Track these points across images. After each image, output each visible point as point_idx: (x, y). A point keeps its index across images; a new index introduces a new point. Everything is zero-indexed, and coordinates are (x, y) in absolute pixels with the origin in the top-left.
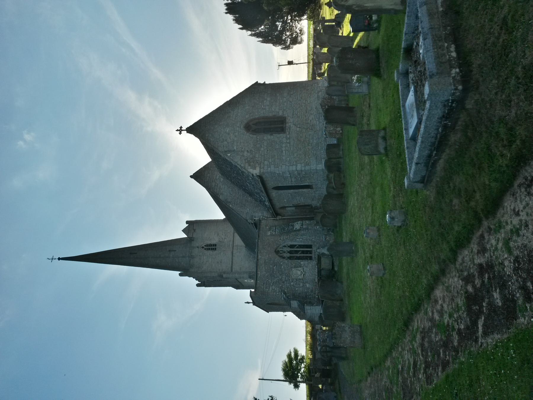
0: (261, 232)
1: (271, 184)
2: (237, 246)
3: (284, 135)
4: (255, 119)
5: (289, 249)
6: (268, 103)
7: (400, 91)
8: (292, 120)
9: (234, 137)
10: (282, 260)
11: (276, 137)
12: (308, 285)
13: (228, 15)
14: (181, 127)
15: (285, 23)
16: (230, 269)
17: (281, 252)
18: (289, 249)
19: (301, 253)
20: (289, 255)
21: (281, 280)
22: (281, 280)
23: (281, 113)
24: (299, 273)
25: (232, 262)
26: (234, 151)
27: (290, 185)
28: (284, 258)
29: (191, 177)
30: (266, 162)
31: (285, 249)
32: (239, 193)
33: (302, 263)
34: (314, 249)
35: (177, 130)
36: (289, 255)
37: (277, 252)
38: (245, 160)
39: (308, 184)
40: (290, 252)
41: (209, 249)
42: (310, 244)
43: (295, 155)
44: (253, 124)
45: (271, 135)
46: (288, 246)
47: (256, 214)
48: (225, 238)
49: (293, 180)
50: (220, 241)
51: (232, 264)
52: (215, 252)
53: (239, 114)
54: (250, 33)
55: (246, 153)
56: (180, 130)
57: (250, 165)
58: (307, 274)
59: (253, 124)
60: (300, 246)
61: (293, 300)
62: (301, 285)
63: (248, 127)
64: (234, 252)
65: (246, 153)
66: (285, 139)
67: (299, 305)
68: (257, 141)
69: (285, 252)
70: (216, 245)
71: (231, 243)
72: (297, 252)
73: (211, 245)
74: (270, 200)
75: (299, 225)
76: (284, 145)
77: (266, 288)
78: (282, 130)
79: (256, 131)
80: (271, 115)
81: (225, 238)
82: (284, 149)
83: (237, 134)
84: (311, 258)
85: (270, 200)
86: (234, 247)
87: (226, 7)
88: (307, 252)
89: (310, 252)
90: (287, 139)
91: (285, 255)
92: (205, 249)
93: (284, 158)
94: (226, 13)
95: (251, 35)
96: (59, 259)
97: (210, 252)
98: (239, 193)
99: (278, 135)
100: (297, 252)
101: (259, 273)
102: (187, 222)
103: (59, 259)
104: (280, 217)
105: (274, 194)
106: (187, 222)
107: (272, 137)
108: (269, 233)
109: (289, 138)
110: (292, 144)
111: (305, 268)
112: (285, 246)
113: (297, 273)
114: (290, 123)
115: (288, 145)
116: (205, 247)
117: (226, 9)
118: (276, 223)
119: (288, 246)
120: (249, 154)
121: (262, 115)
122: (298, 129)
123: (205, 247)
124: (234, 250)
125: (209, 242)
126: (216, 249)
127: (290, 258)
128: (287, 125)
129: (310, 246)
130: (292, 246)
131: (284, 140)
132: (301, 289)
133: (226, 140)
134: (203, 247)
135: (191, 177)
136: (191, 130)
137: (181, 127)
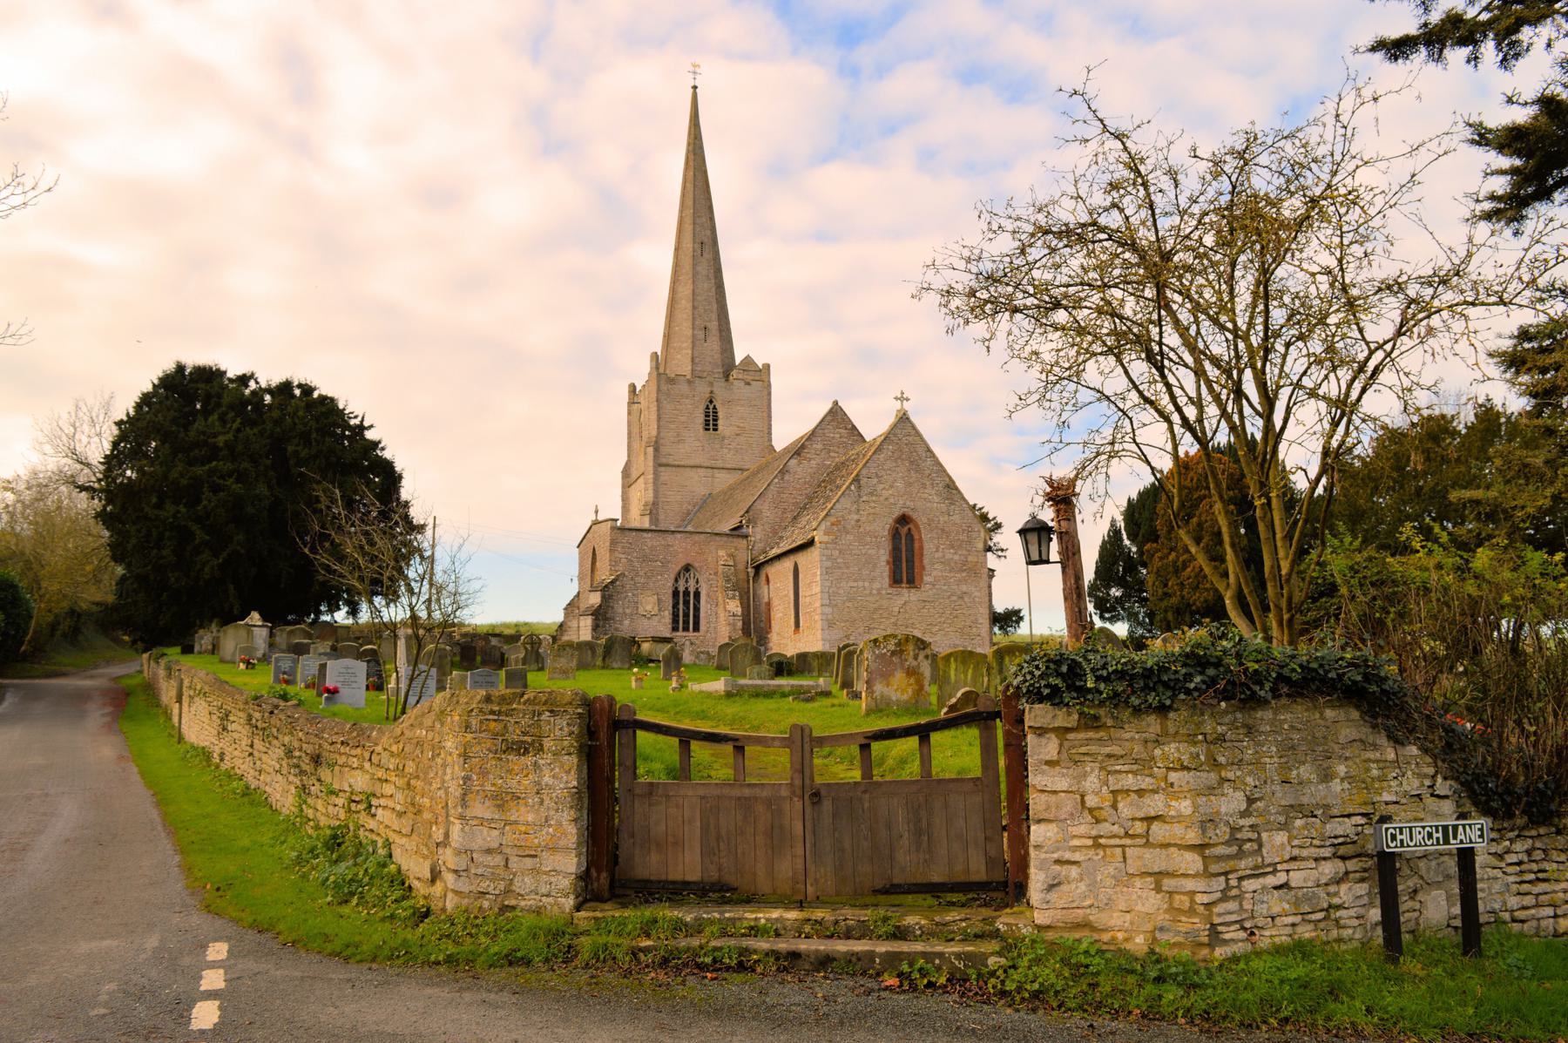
1: (801, 558)
5: (692, 590)
6: (948, 556)
7: (1003, 778)
8: (913, 598)
9: (894, 493)
11: (883, 571)
12: (627, 622)
16: (664, 461)
18: (692, 590)
19: (685, 609)
20: (681, 589)
21: (637, 575)
22: (637, 575)
24: (649, 608)
29: (836, 403)
30: (836, 553)
31: (692, 583)
34: (691, 634)
35: (1468, 61)
36: (681, 589)
37: (687, 568)
40: (686, 593)
42: (703, 627)
47: (758, 529)
56: (902, 398)
60: (697, 609)
61: (603, 597)
63: (904, 520)
71: (719, 464)
72: (686, 603)
73: (715, 420)
74: (779, 557)
78: (896, 580)
79: (895, 535)
80: (926, 561)
84: (675, 629)
85: (779, 557)
88: (686, 622)
89: (686, 629)
91: (681, 583)
93: (843, 584)
96: (695, 87)
97: (701, 419)
99: (886, 574)
100: (686, 603)
102: (767, 367)
103: (695, 87)
105: (787, 564)
106: (767, 367)
113: (648, 604)
114: (906, 595)
118: (741, 567)
121: (926, 546)
125: (720, 415)
127: (676, 593)
129: (696, 629)
130: (697, 595)
131: (877, 585)
135: (836, 403)
136: (903, 419)
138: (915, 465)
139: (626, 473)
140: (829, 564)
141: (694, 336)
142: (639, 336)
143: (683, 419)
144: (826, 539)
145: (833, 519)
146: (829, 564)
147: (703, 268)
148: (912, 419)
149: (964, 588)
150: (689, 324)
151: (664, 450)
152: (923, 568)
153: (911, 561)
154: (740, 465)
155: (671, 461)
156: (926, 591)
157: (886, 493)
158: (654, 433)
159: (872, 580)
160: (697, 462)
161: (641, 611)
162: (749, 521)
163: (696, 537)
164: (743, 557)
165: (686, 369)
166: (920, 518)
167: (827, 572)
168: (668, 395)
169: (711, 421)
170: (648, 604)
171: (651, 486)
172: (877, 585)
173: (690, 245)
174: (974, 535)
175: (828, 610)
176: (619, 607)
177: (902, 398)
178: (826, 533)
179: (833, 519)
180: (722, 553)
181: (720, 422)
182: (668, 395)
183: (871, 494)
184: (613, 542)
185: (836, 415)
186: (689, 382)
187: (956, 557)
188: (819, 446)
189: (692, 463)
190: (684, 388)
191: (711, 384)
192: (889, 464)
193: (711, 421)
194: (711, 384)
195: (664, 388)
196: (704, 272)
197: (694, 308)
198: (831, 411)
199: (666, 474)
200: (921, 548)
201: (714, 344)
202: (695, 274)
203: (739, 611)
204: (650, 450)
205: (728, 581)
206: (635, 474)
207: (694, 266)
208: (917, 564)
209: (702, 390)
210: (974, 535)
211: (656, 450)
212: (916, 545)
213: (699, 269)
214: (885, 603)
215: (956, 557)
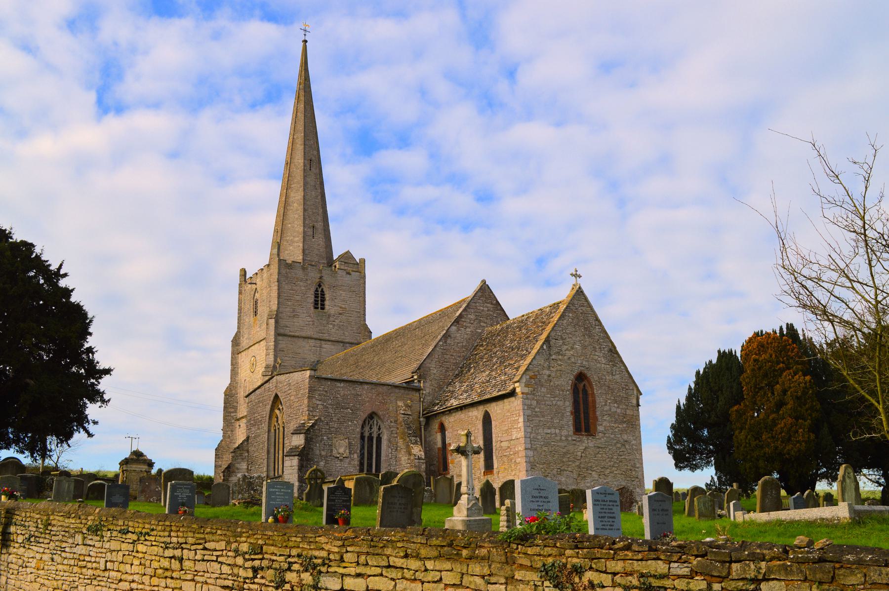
0: (403, 391)
1: (495, 409)
2: (321, 347)
3: (571, 433)
4: (592, 389)
5: (375, 435)
6: (614, 409)
8: (591, 445)
9: (575, 354)
10: (361, 422)
11: (569, 420)
13: (717, 355)
14: (580, 277)
15: (706, 441)
16: (282, 331)
17: (371, 422)
18: (375, 435)
20: (367, 434)
23: (600, 428)
24: (341, 450)
25: (316, 339)
26: (550, 355)
27: (494, 440)
28: (363, 427)
29: (484, 282)
31: (375, 429)
32: (459, 357)
33: (356, 456)
36: (367, 434)
37: (372, 416)
38: (538, 371)
39: (495, 466)
40: (371, 438)
41: (316, 296)
43: (545, 449)
44: (584, 385)
45: (572, 413)
46: (379, 435)
47: (427, 384)
48: (334, 325)
49: (504, 444)
50: (329, 316)
51: (290, 336)
52: (311, 306)
53: (598, 365)
54: (693, 386)
55: (548, 372)
57: (531, 378)
58: (338, 463)
59: (584, 385)
61: (306, 439)
62: (323, 453)
64: (310, 341)
65: (548, 372)
66: (566, 433)
67: (297, 447)
68: (563, 391)
69: (371, 428)
70: (323, 309)
71: (326, 336)
73: (323, 300)
74: (462, 408)
75: (419, 454)
76: (557, 431)
77: (319, 395)
78: (577, 430)
79: (575, 390)
80: (598, 413)
81: (334, 325)
82: (553, 430)
83: (573, 360)
86: (319, 342)
87: (727, 351)
90: (566, 436)
91: (367, 428)
92: (317, 290)
93: (540, 431)
94: (719, 351)
95: (690, 388)
96: (305, 41)
97: (311, 299)
98: (459, 357)
99: (571, 423)
101: (342, 385)
102: (363, 261)
104: (423, 423)
105: (477, 414)
107: (569, 414)
108: (400, 403)
109: (567, 440)
110: (559, 444)
111: (347, 460)
112: (379, 429)
113: (341, 447)
114: (588, 442)
115: (558, 438)
116: (320, 290)
117: (724, 352)
119: (379, 435)
120: (546, 377)
122: (579, 454)
123: (320, 290)
124: (313, 341)
125: (327, 297)
126: (316, 308)
128: (585, 438)
131: (564, 433)
132: (318, 452)
133: (564, 343)
134: (320, 286)
135: (484, 282)
136: (579, 293)
137: (580, 277)
138: (588, 332)
139: (236, 342)
140: (529, 412)
141: (304, 232)
142: (251, 235)
143: (298, 298)
144: (526, 390)
145: (531, 373)
146: (529, 412)
147: (311, 180)
148: (586, 292)
149: (625, 437)
150: (301, 222)
151: (282, 322)
152: (596, 419)
153: (586, 414)
154: (342, 338)
155: (287, 332)
156: (600, 439)
157: (569, 353)
158: (275, 307)
159: (561, 428)
160: (309, 333)
161: (335, 452)
162: (420, 377)
163: (380, 389)
164: (419, 407)
165: (299, 258)
166: (594, 377)
167: (528, 419)
168: (287, 277)
169: (319, 302)
170: (341, 447)
171: (272, 352)
172: (564, 433)
173: (301, 161)
174: (630, 392)
175: (530, 453)
176: (318, 449)
177: (576, 275)
178: (527, 385)
179: (531, 373)
180: (400, 403)
181: (327, 303)
182: (287, 277)
183: (558, 353)
184: (311, 390)
185: (484, 292)
186: (304, 268)
187: (619, 411)
188: (472, 317)
189: (303, 334)
190: (299, 273)
191: (320, 271)
192: (570, 329)
193: (319, 302)
194: (320, 271)
195: (283, 271)
196: (312, 183)
197: (305, 210)
198: (481, 289)
199: (284, 343)
200: (594, 402)
201: (320, 240)
202: (305, 184)
203: (422, 454)
204: (272, 321)
205: (409, 428)
206: (244, 342)
207: (305, 177)
208: (591, 415)
209: (314, 275)
210: (630, 392)
211: (276, 322)
212: (590, 399)
213: (308, 180)
214: (571, 448)
215: (619, 411)
